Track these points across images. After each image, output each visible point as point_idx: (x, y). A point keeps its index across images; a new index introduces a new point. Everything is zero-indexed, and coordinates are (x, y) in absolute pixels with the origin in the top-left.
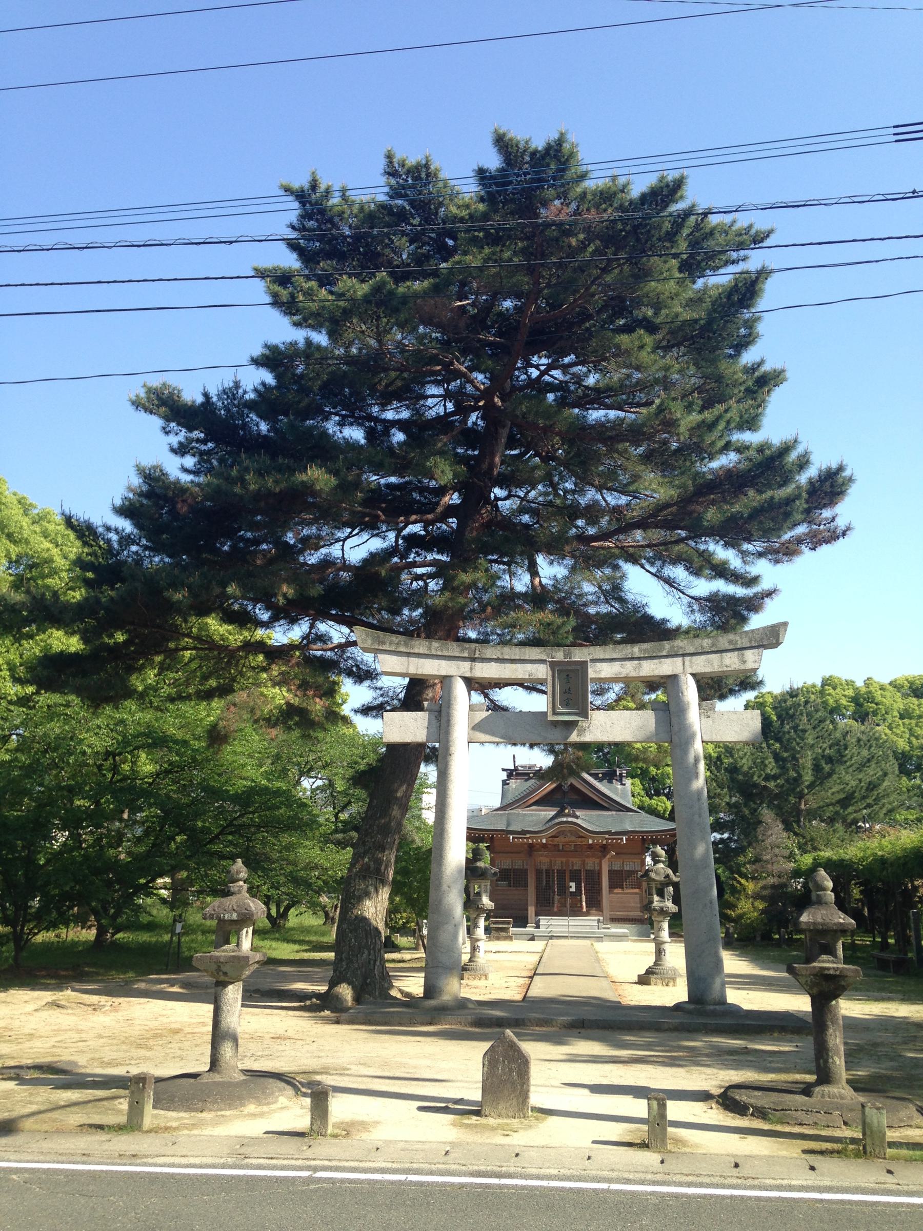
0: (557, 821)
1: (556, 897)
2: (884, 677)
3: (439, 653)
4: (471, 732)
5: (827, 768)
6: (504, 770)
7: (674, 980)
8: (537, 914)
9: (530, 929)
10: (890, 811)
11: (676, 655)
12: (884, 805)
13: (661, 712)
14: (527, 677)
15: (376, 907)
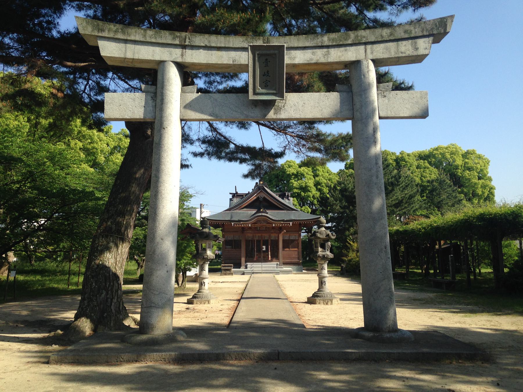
0: (256, 215)
1: (256, 253)
2: (410, 152)
3: (153, 40)
4: (183, 110)
5: (390, 188)
6: (230, 194)
7: (331, 301)
8: (246, 262)
9: (242, 269)
10: (414, 211)
11: (359, 44)
12: (413, 207)
13: (345, 94)
14: (231, 63)
15: (116, 259)
